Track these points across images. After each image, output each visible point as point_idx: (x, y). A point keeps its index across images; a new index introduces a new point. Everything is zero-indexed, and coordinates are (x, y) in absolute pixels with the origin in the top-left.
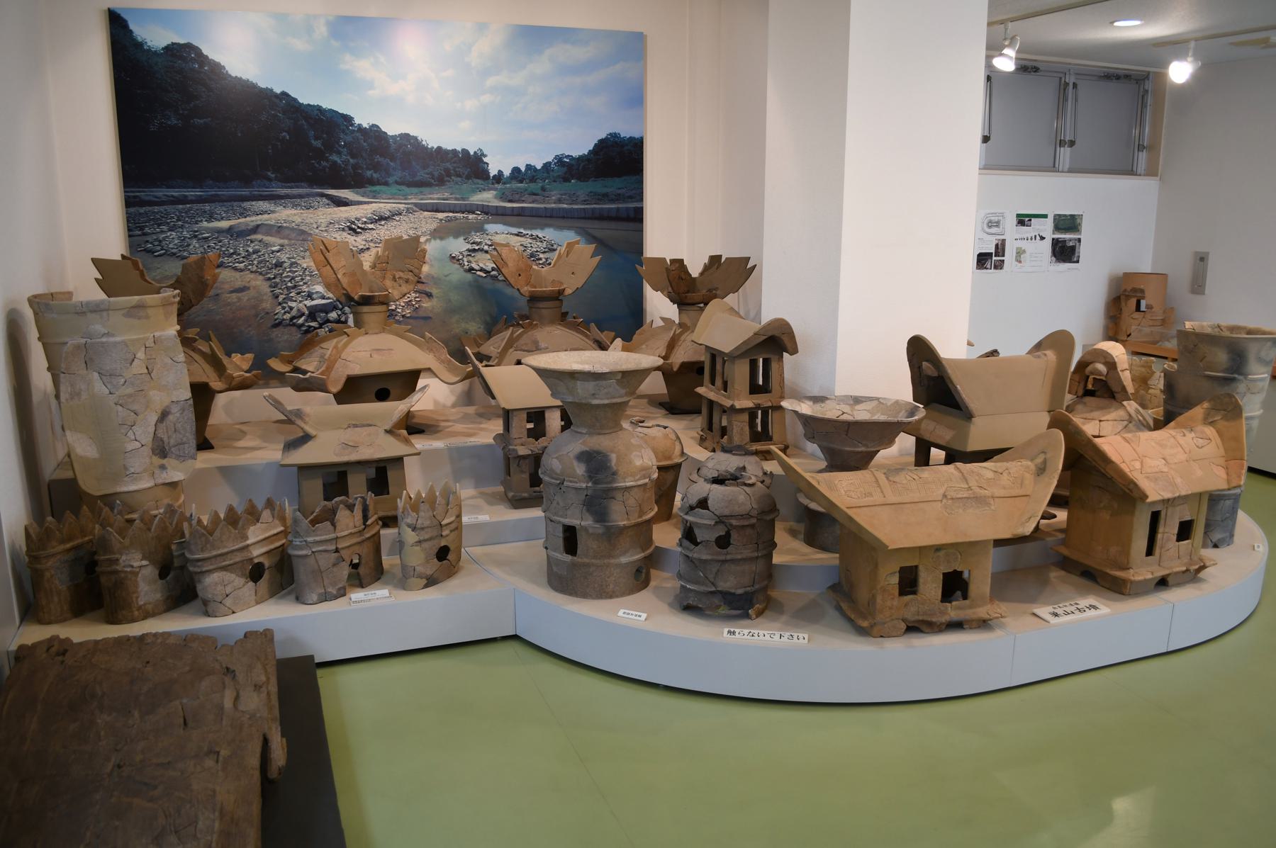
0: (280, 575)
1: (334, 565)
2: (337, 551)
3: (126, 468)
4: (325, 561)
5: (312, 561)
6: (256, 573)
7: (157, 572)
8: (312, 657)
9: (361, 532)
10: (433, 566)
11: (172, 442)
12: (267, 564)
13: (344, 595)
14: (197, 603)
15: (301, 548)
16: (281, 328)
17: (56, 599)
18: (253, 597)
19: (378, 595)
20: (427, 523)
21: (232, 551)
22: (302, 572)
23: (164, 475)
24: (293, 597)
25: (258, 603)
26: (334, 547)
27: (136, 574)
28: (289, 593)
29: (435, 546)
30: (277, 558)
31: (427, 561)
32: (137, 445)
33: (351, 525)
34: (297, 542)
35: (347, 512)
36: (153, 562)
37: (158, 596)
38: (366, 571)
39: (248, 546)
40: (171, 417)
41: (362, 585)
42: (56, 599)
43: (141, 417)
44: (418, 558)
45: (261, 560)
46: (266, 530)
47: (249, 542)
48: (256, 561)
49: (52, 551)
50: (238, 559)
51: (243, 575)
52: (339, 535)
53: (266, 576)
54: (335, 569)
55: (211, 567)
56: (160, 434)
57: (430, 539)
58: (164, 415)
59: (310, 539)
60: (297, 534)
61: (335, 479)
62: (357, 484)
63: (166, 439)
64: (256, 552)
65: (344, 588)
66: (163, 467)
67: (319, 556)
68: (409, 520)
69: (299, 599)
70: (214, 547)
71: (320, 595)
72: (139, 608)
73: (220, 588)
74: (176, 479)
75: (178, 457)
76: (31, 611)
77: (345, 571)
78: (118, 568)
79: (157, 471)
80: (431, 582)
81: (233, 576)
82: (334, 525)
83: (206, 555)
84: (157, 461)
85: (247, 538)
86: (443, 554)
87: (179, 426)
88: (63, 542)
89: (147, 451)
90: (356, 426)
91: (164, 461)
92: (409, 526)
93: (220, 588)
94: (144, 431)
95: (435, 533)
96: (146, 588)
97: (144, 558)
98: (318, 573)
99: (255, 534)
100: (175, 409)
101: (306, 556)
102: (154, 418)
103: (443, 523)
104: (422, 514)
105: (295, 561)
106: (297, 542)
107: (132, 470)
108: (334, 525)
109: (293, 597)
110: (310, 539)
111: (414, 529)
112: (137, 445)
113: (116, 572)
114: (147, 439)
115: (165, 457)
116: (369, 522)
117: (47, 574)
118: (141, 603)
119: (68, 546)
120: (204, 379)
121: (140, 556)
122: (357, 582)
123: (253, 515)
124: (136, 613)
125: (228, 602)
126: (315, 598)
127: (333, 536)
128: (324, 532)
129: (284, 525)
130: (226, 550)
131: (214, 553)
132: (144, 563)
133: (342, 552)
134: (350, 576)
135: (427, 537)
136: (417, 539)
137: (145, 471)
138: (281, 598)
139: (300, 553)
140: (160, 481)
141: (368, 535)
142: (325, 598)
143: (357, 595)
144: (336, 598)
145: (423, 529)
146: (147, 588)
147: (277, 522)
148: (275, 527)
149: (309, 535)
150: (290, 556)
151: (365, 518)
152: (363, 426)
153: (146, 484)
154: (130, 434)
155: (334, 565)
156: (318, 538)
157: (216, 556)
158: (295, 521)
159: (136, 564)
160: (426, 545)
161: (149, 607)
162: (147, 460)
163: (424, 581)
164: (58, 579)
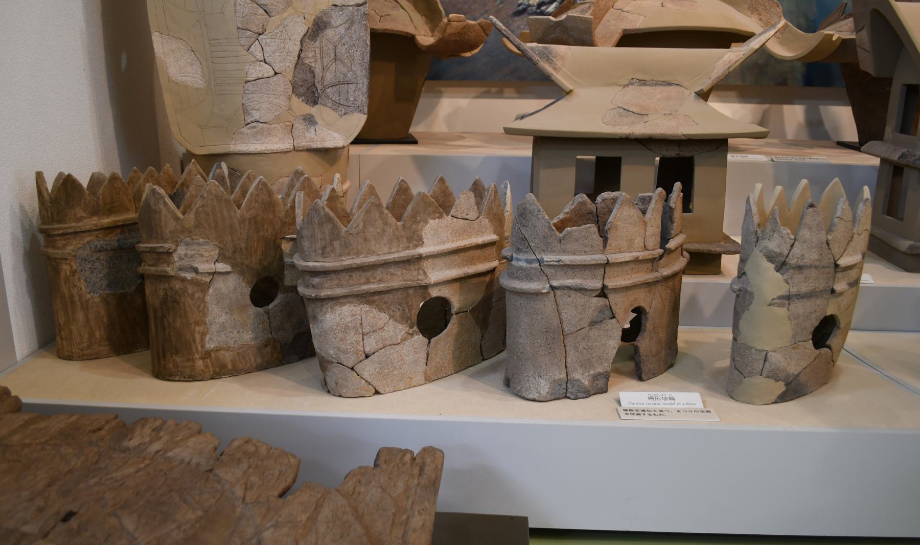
0: (477, 327)
1: (593, 323)
2: (603, 293)
3: (246, 112)
4: (576, 311)
5: (548, 306)
6: (431, 318)
7: (247, 290)
8: (525, 520)
9: (653, 262)
10: (797, 360)
11: (329, 77)
12: (456, 303)
13: (604, 390)
14: (314, 363)
15: (528, 276)
16: (524, 16)
17: (80, 316)
18: (422, 367)
19: (668, 404)
20: (812, 256)
21: (386, 264)
22: (524, 326)
23: (311, 134)
24: (499, 377)
25: (429, 379)
26: (598, 285)
27: (204, 287)
28: (493, 369)
29: (811, 312)
30: (479, 297)
31: (795, 345)
32: (267, 70)
33: (639, 242)
34: (521, 261)
35: (634, 212)
36: (239, 268)
37: (248, 337)
38: (645, 349)
39: (420, 258)
40: (329, 32)
41: (639, 375)
42: (80, 316)
43: (276, 20)
44: (777, 334)
45: (444, 292)
46: (460, 234)
47: (422, 250)
48: (434, 293)
49: (73, 225)
50: (395, 283)
51: (404, 319)
52: (615, 258)
53: (453, 326)
54: (594, 333)
55: (339, 291)
56: (309, 58)
57: (810, 295)
58: (318, 27)
59: (549, 258)
60: (522, 244)
61: (602, 163)
62: (639, 175)
63: (318, 70)
64: (437, 274)
65: (606, 376)
66: (310, 120)
67: (564, 299)
68: (773, 245)
69: (511, 385)
70: (347, 249)
71: (555, 383)
72: (207, 354)
73: (352, 337)
74: (329, 144)
75: (336, 106)
76: (51, 338)
77: (610, 341)
78: (170, 271)
79: (299, 126)
80: (793, 390)
81: (384, 316)
82: (604, 235)
83: (329, 264)
84: (300, 106)
85: (420, 242)
86: (824, 332)
87: (342, 50)
88: (95, 211)
89: (282, 85)
90: (643, 83)
91: (313, 110)
92: (770, 258)
93: (352, 337)
94: (282, 46)
95: (821, 285)
96: (223, 318)
97: (222, 258)
98: (559, 335)
99: (436, 236)
100: (337, 19)
101: (537, 294)
102: (300, 29)
103: (843, 262)
104: (805, 233)
105: (513, 306)
106: (521, 261)
107: (256, 115)
108: (604, 235)
109: (499, 377)
110: (549, 258)
111: (781, 266)
112: (267, 70)
113: (165, 278)
114: (286, 64)
115: (315, 103)
116: (672, 244)
117: (65, 268)
118: (210, 346)
119: (106, 221)
120: (410, 30)
121: (215, 253)
122: (631, 365)
123: (443, 203)
124: (200, 364)
125: (368, 369)
126: (544, 387)
127: (600, 258)
128: (582, 247)
129: (500, 233)
130: (372, 259)
131: (347, 262)
132: (222, 267)
133: (612, 297)
134: (620, 352)
135: (804, 288)
136: (783, 290)
137: (278, 119)
138: (478, 375)
139: (532, 286)
140: (304, 143)
141: (666, 272)
142: (566, 391)
143: (632, 395)
144: (587, 393)
145: (800, 268)
146: (225, 317)
147: (486, 222)
148: (481, 232)
149: (547, 249)
150: (503, 291)
151: (665, 238)
152: (657, 83)
153: (278, 143)
154: (256, 49)
155: (593, 323)
156: (567, 259)
157: (350, 270)
158: (523, 214)
159: (203, 267)
160: (799, 307)
161: (227, 357)
162: (283, 101)
163: (780, 388)
164: (88, 286)
